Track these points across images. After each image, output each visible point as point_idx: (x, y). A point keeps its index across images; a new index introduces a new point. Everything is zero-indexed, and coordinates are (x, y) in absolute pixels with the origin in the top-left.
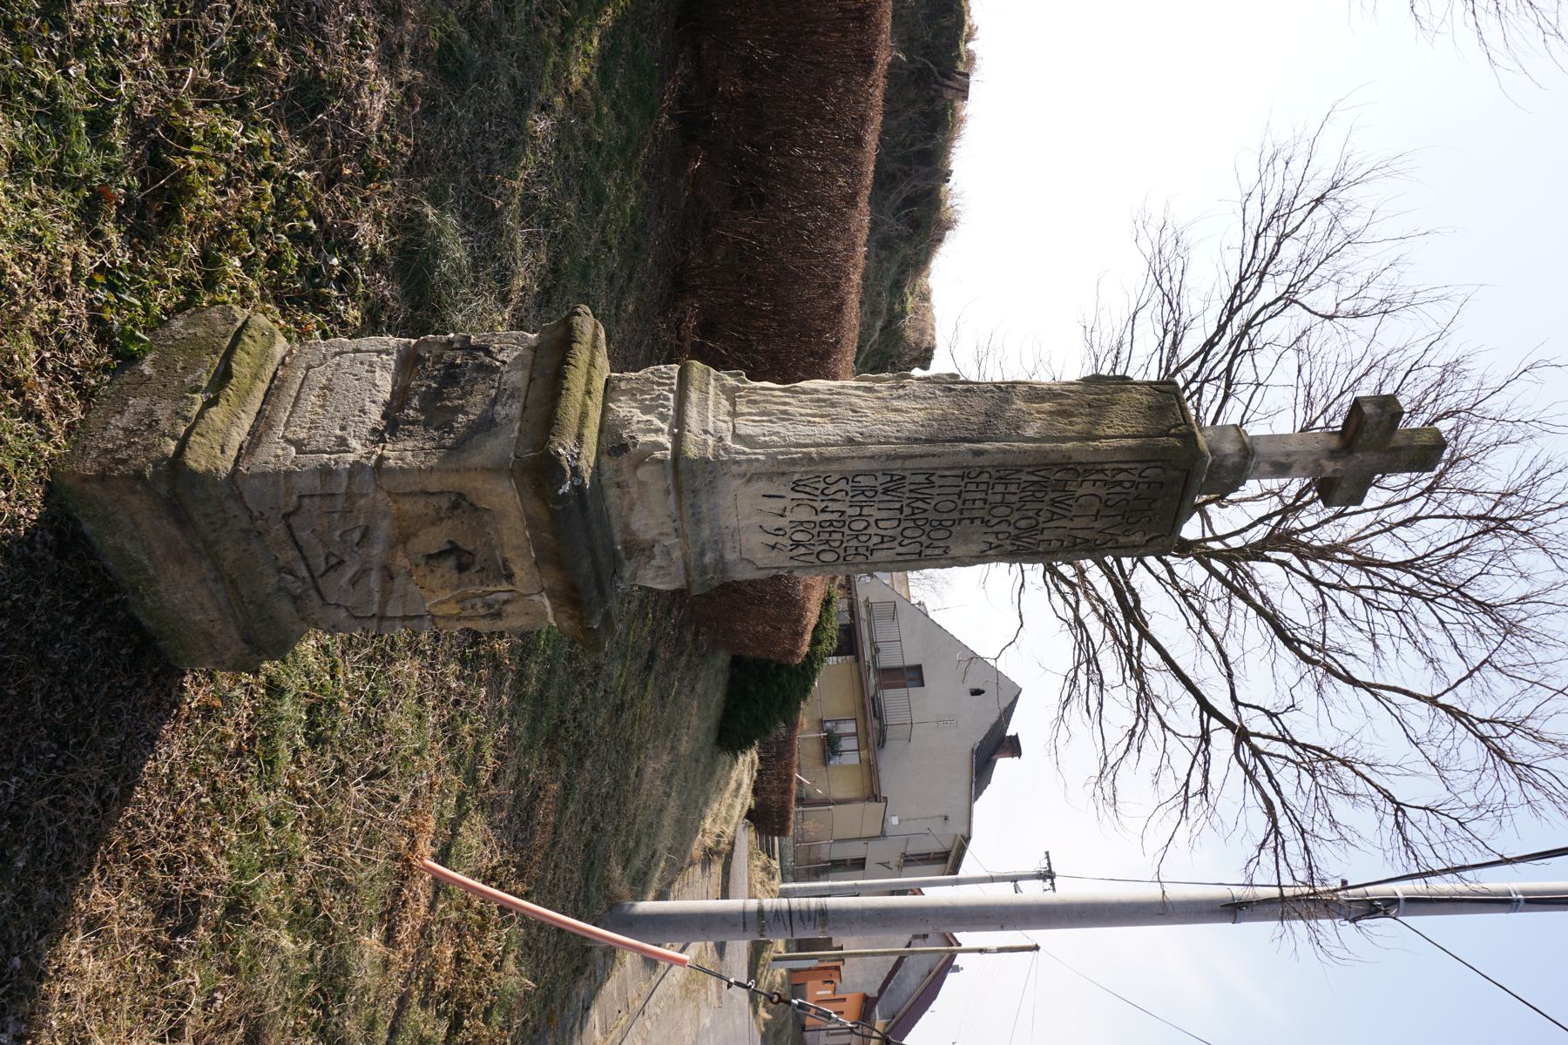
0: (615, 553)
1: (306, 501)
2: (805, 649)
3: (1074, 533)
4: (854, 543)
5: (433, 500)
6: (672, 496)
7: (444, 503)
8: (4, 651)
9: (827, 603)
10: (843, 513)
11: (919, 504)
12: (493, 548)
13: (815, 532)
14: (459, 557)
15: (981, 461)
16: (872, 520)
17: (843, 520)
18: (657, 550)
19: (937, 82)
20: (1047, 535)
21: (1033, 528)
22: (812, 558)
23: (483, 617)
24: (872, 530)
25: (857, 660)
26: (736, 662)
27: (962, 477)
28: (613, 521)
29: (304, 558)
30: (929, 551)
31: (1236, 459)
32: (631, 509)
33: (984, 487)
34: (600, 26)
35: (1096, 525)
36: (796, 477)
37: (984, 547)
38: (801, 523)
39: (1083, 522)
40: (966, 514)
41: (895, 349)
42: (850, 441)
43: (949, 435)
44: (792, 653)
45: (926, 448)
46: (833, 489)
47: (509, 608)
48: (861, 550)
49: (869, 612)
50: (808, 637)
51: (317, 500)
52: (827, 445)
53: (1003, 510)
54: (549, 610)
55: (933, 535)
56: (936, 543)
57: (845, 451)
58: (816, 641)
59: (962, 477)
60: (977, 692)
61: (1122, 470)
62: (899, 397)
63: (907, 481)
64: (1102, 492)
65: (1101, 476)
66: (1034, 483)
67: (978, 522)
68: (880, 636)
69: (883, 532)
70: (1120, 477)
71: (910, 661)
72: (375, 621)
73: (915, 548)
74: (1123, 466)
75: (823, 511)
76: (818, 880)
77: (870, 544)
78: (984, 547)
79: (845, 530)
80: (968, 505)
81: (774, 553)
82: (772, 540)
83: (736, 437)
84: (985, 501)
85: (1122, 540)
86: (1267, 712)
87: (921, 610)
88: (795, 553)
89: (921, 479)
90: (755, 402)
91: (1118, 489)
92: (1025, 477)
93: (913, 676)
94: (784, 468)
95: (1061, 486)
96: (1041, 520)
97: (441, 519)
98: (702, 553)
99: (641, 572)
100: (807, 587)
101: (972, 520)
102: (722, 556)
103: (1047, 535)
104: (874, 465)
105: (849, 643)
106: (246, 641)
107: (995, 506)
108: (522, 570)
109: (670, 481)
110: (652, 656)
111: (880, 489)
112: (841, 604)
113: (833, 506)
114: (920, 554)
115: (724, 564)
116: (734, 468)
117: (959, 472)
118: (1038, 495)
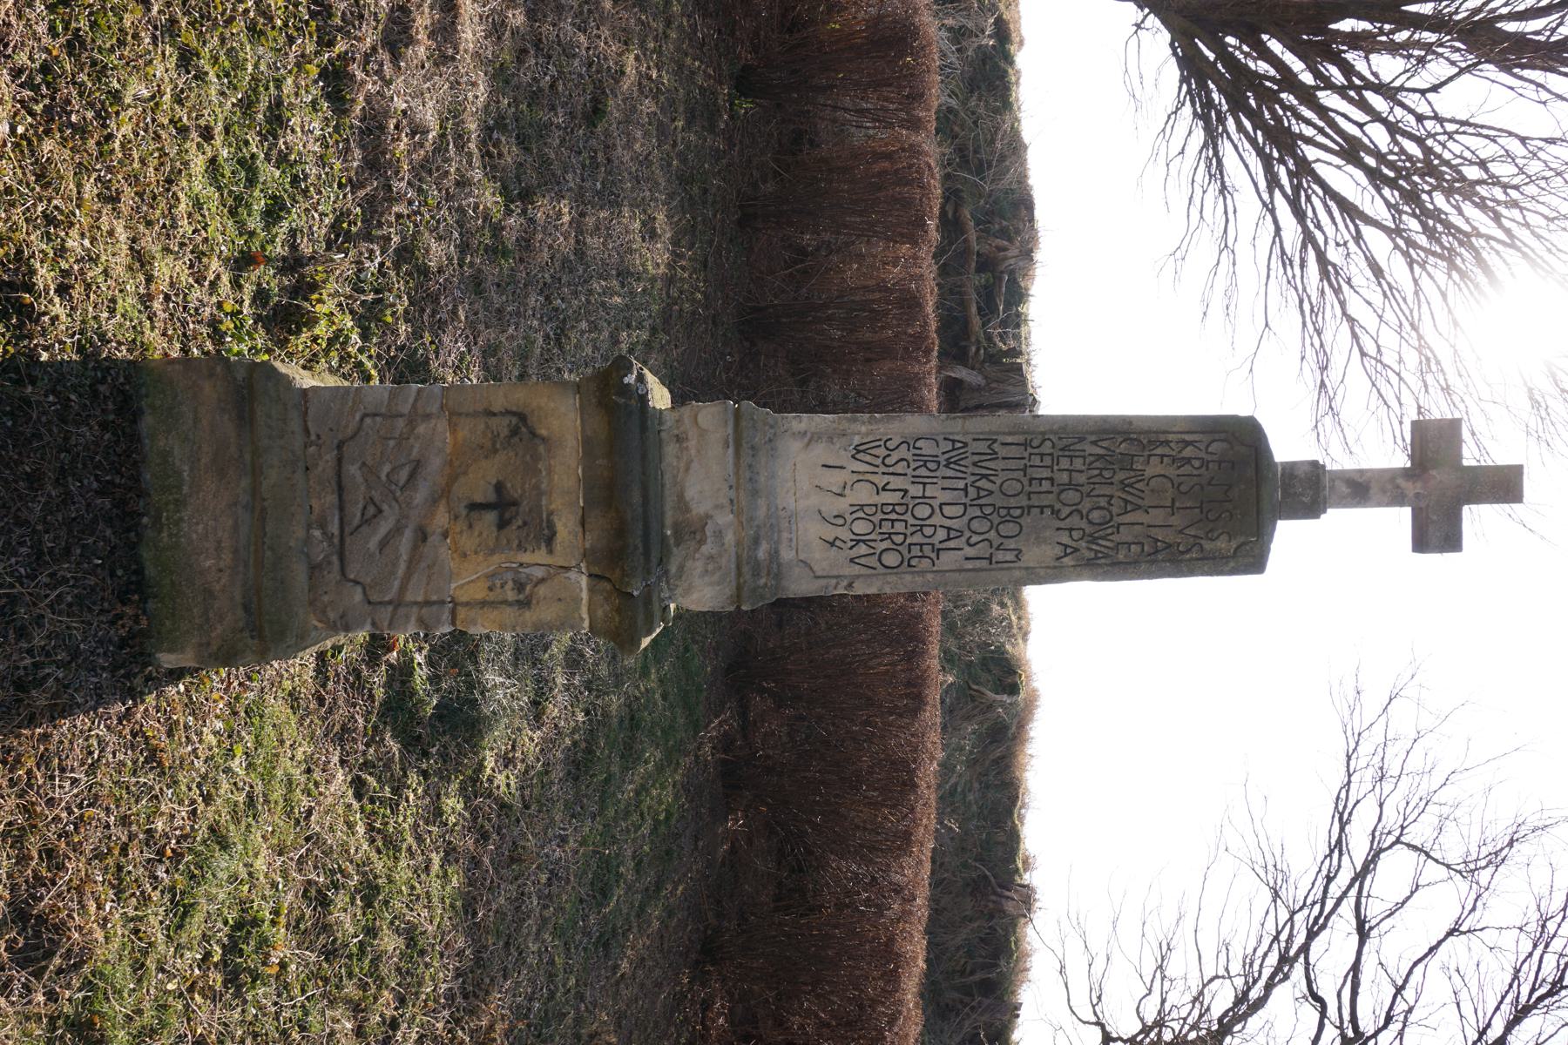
0: (664, 538)
1: (368, 421)
5: (494, 422)
6: (731, 450)
7: (502, 425)
10: (906, 491)
11: (982, 483)
12: (540, 494)
14: (502, 506)
16: (936, 503)
18: (709, 531)
19: (995, 893)
20: (1125, 535)
23: (510, 604)
27: (1025, 445)
28: (667, 492)
29: (341, 509)
30: (1000, 556)
32: (687, 469)
35: (1175, 520)
36: (857, 440)
37: (1059, 551)
47: (542, 590)
51: (378, 419)
54: (585, 595)
59: (1025, 445)
63: (970, 449)
64: (1172, 472)
65: (1166, 451)
67: (1048, 512)
69: (948, 523)
72: (390, 608)
74: (1188, 437)
76: (888, 958)
77: (935, 540)
79: (908, 517)
84: (1051, 479)
95: (1127, 462)
96: (1115, 510)
97: (496, 451)
99: (689, 564)
102: (777, 552)
106: (246, 608)
108: (566, 527)
109: (730, 430)
111: (942, 459)
113: (896, 482)
114: (990, 559)
115: (779, 565)
118: (1107, 474)
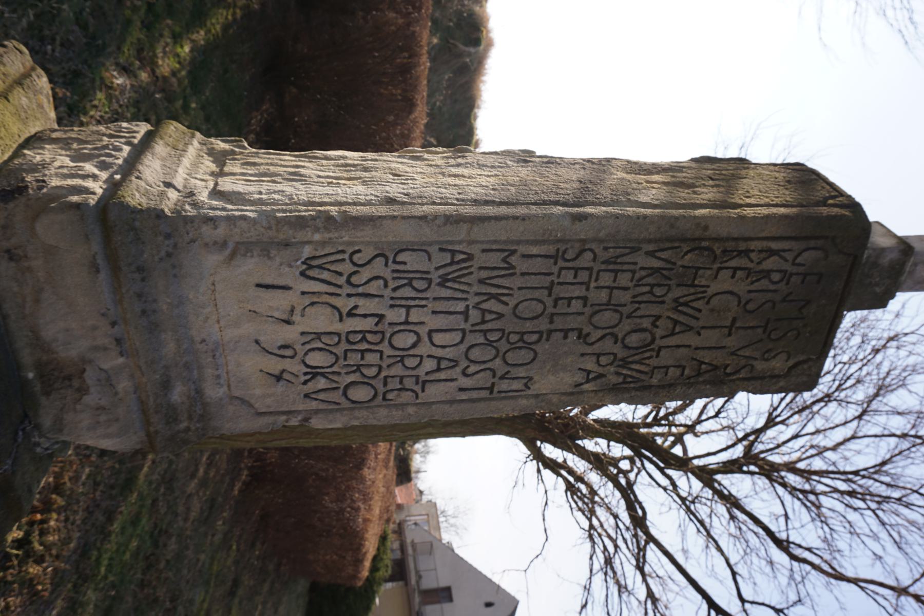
2: (365, 573)
3: (700, 355)
4: (397, 370)
6: (103, 276)
8: (74, 605)
9: (383, 538)
10: (381, 317)
13: (339, 351)
15: (582, 231)
16: (423, 331)
17: (381, 331)
18: (90, 376)
20: (666, 358)
21: (646, 346)
22: (336, 396)
24: (424, 349)
25: (406, 584)
26: (314, 588)
27: (554, 257)
30: (504, 385)
31: (894, 255)
33: (583, 276)
34: (193, 41)
35: (730, 342)
36: (307, 251)
37: (579, 377)
38: (318, 336)
39: (711, 337)
40: (559, 323)
41: (454, 128)
42: (391, 201)
43: (533, 198)
44: (355, 577)
45: (503, 210)
46: (366, 274)
48: (409, 383)
49: (414, 550)
50: (367, 564)
52: (355, 204)
53: (608, 318)
55: (510, 357)
56: (515, 372)
57: (383, 210)
58: (374, 569)
60: (489, 605)
61: (772, 253)
62: (458, 165)
63: (476, 263)
64: (741, 288)
66: (654, 271)
67: (573, 336)
68: (422, 567)
69: (439, 352)
70: (771, 263)
71: (443, 584)
73: (483, 379)
74: (774, 245)
75: (350, 314)
77: (421, 372)
78: (579, 377)
80: (562, 308)
81: (280, 388)
82: (275, 365)
83: (216, 193)
85: (760, 366)
86: (773, 608)
87: (449, 548)
88: (310, 387)
89: (495, 259)
90: (254, 164)
91: (764, 284)
92: (643, 261)
93: (444, 594)
94: (287, 233)
96: (659, 332)
98: (166, 385)
100: (366, 521)
101: (566, 333)
102: (199, 392)
103: (666, 358)
104: (428, 233)
105: (400, 572)
107: (600, 308)
110: (236, 583)
111: (435, 277)
112: (393, 543)
113: (366, 306)
114: (491, 389)
116: (206, 230)
117: (550, 249)
118: (658, 291)
